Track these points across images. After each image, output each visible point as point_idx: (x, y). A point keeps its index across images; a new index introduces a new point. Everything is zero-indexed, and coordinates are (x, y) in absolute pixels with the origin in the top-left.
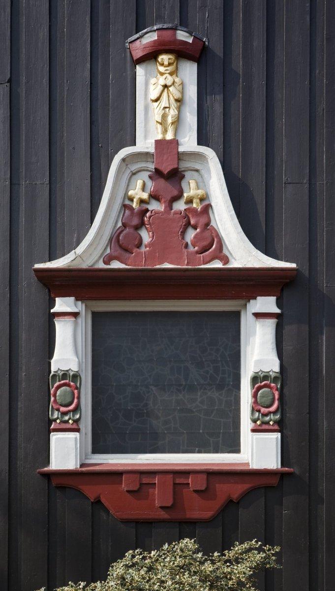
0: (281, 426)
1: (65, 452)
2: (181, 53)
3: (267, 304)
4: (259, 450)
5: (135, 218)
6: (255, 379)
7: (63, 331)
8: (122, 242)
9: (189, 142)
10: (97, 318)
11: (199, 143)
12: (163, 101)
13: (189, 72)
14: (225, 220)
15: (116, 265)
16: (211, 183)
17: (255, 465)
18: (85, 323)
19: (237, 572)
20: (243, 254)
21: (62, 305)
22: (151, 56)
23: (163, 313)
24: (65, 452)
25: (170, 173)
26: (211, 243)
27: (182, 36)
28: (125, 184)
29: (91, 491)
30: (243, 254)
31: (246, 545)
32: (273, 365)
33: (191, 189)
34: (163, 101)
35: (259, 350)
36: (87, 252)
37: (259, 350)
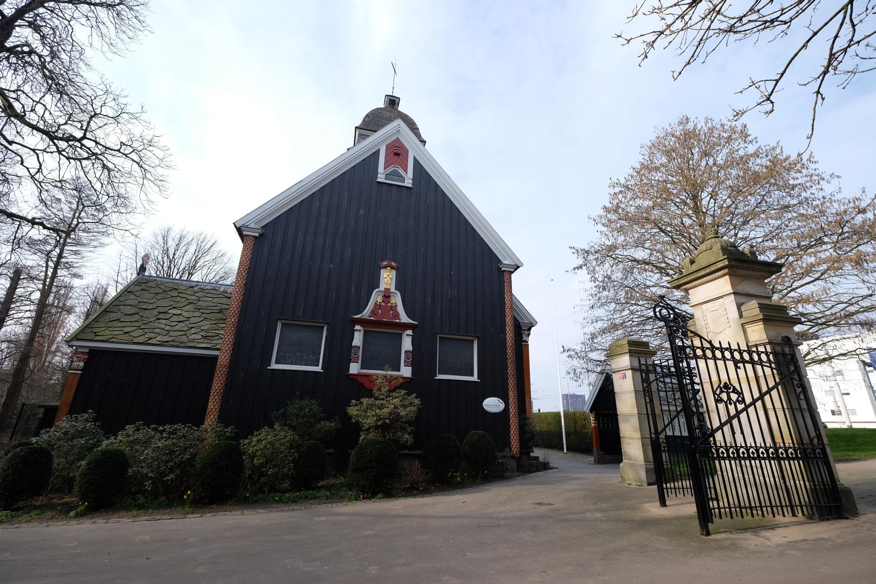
0: (412, 365)
1: (354, 368)
2: (392, 268)
3: (410, 332)
4: (406, 371)
5: (377, 306)
6: (406, 352)
7: (356, 334)
8: (373, 313)
9: (393, 289)
10: (365, 331)
11: (406, 352)
12: (388, 278)
13: (394, 272)
14: (401, 309)
16: (397, 300)
17: (405, 375)
18: (362, 333)
19: (728, 200)
20: (404, 318)
21: (357, 327)
22: (385, 267)
23: (383, 329)
24: (354, 368)
25: (387, 296)
26: (397, 315)
27: (393, 264)
28: (376, 298)
29: (360, 380)
30: (404, 318)
31: (833, 311)
32: (410, 348)
33: (393, 301)
34: (388, 278)
35: (407, 344)
36: (366, 313)
37: (407, 344)
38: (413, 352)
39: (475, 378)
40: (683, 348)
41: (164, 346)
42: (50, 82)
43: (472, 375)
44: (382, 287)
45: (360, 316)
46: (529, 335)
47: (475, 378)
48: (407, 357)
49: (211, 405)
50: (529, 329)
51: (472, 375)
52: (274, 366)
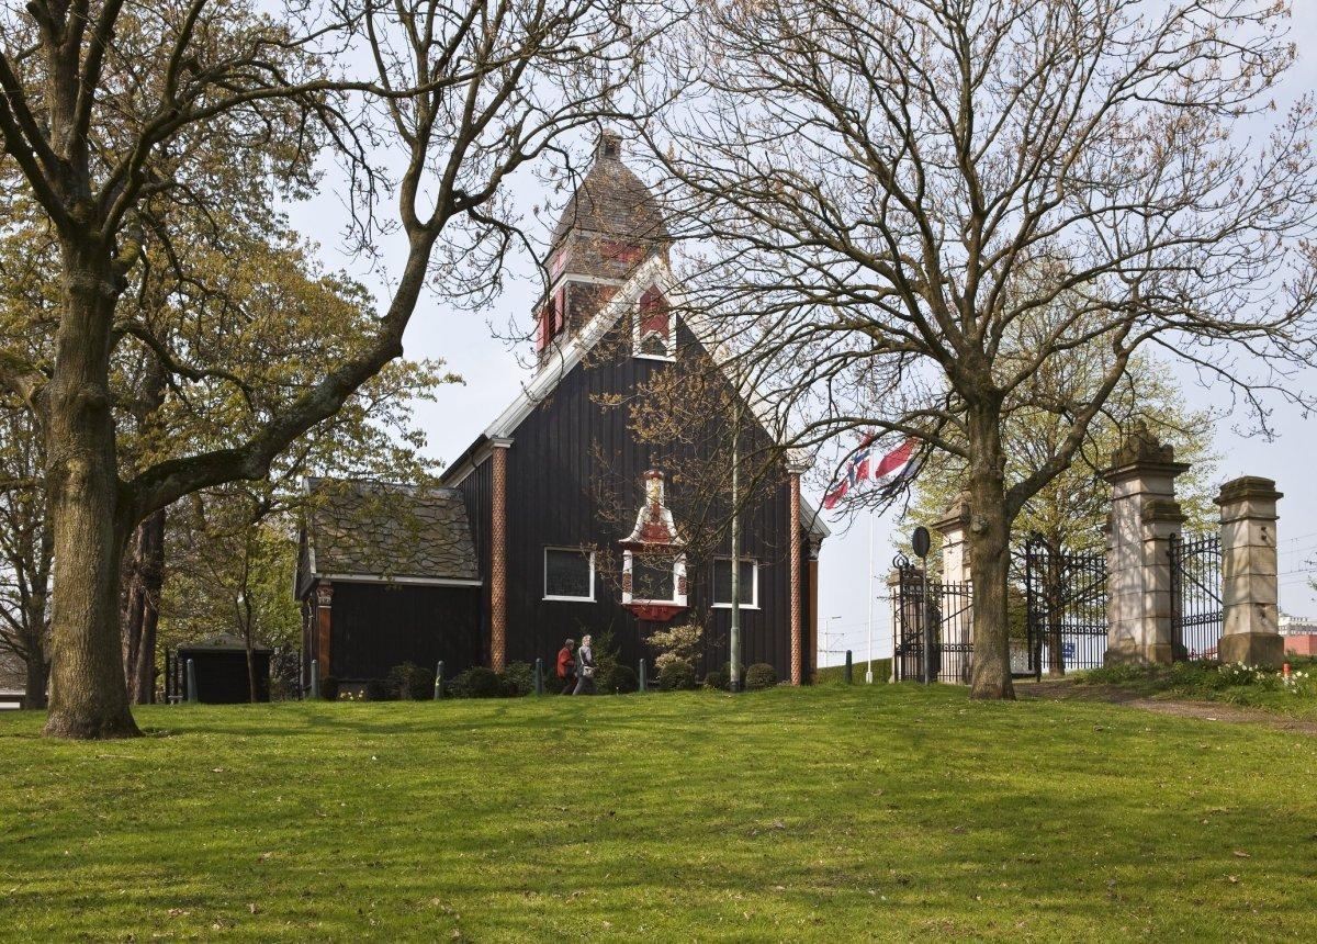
1: (627, 598)
2: (659, 477)
8: (643, 534)
12: (654, 488)
14: (671, 524)
21: (626, 552)
22: (653, 476)
24: (627, 598)
25: (656, 515)
28: (643, 515)
34: (654, 488)
35: (680, 570)
37: (680, 570)
39: (591, 598)
40: (1036, 556)
42: (350, 286)
43: (751, 602)
45: (628, 540)
46: (819, 549)
47: (591, 598)
48: (681, 587)
49: (496, 558)
50: (820, 541)
51: (751, 602)
52: (549, 598)
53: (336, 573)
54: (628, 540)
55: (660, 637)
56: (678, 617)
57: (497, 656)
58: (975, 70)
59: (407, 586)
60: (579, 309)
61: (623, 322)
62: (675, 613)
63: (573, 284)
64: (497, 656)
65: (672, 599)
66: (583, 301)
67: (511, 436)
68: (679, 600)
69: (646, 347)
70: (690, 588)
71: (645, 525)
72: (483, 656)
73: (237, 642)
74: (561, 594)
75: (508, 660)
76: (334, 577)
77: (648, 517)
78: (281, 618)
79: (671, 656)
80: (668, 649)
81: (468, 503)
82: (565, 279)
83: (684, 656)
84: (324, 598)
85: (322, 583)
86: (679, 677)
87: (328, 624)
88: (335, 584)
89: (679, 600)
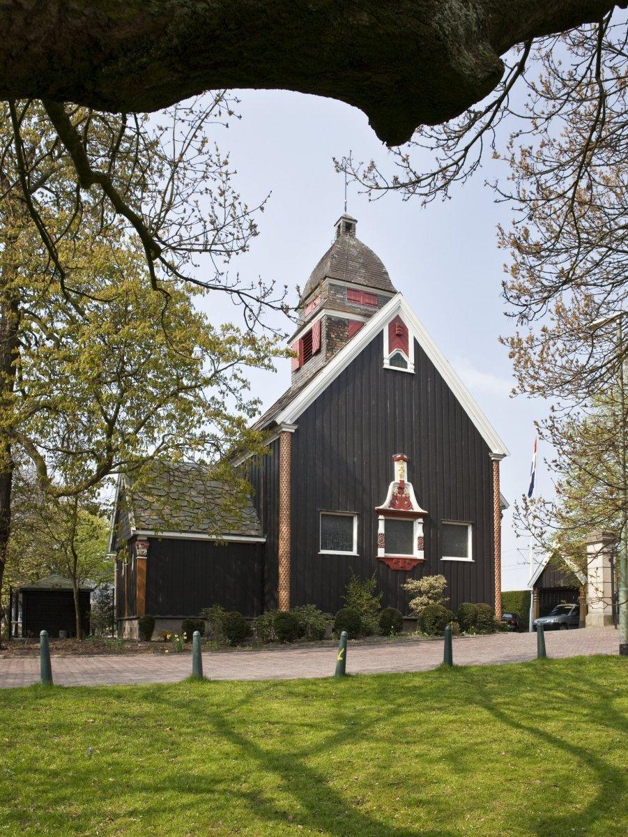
1: (381, 553)
2: (404, 460)
3: (421, 520)
8: (392, 504)
12: (400, 470)
15: (391, 509)
16: (410, 490)
20: (417, 508)
21: (381, 517)
22: (398, 460)
24: (381, 553)
25: (401, 487)
26: (410, 505)
28: (392, 489)
30: (417, 508)
32: (422, 535)
34: (400, 470)
35: (418, 531)
37: (418, 531)
38: (424, 538)
39: (354, 552)
41: (204, 533)
43: (466, 556)
44: (397, 479)
51: (466, 556)
52: (445, 558)
53: (165, 531)
54: (381, 507)
55: (411, 585)
56: (419, 569)
57: (284, 595)
58: (457, 177)
59: (232, 543)
60: (333, 336)
61: (377, 341)
62: (415, 564)
63: (329, 318)
64: (284, 595)
65: (411, 552)
66: (338, 332)
67: (296, 423)
68: (418, 554)
69: (392, 362)
70: (426, 544)
71: (394, 497)
72: (266, 597)
73: (67, 583)
74: (331, 549)
75: (293, 602)
76: (166, 534)
77: (396, 490)
78: (102, 571)
79: (424, 599)
80: (420, 593)
81: (253, 479)
82: (323, 313)
83: (435, 600)
84: (142, 550)
85: (139, 538)
86: (437, 617)
87: (145, 568)
88: (150, 539)
89: (418, 554)
